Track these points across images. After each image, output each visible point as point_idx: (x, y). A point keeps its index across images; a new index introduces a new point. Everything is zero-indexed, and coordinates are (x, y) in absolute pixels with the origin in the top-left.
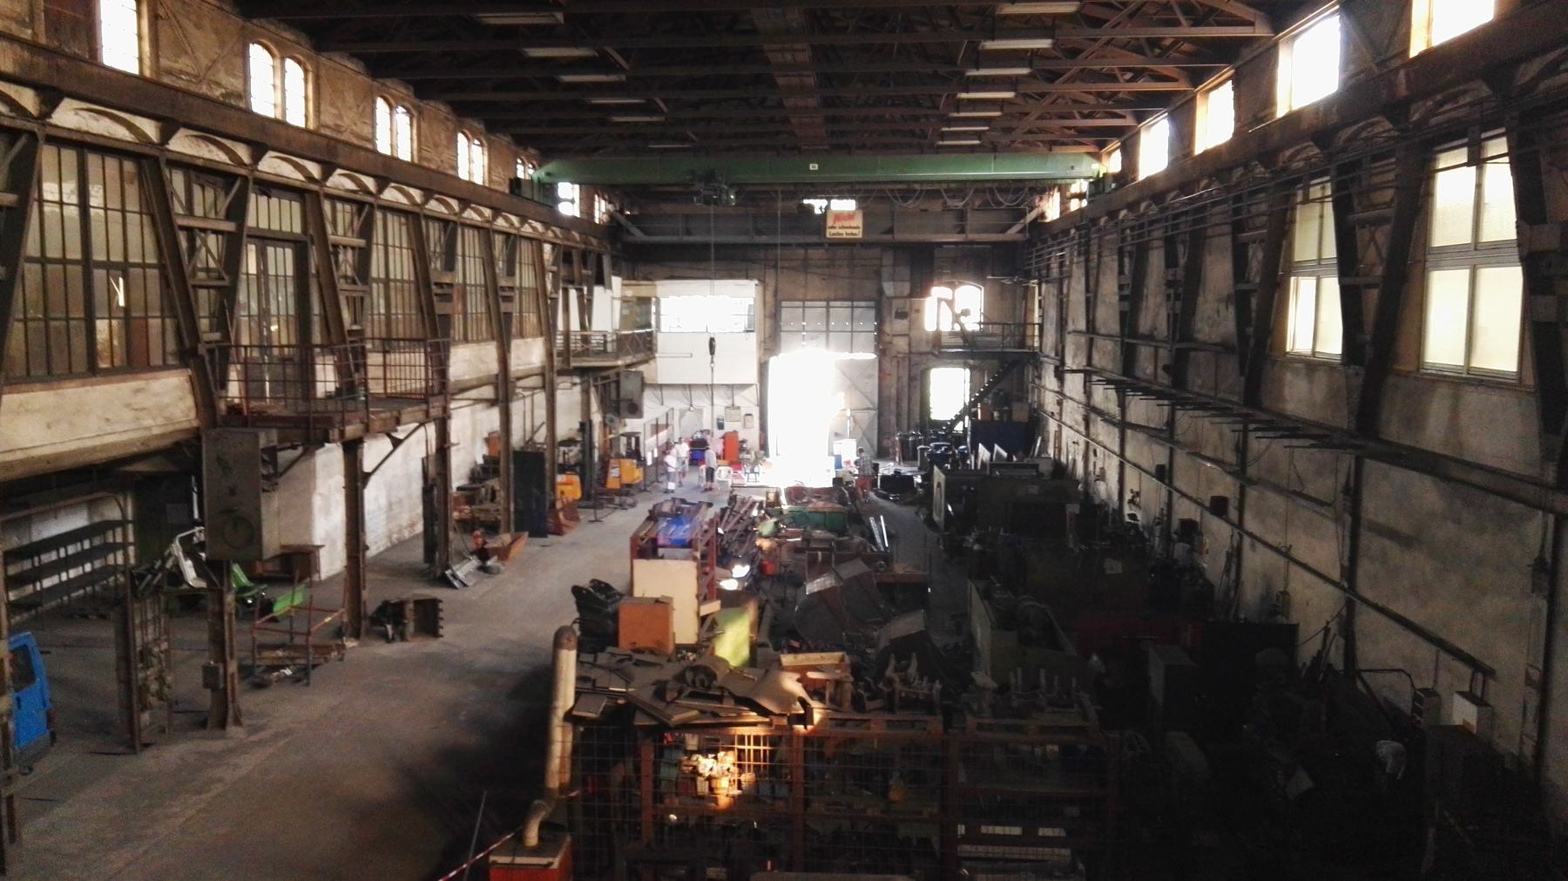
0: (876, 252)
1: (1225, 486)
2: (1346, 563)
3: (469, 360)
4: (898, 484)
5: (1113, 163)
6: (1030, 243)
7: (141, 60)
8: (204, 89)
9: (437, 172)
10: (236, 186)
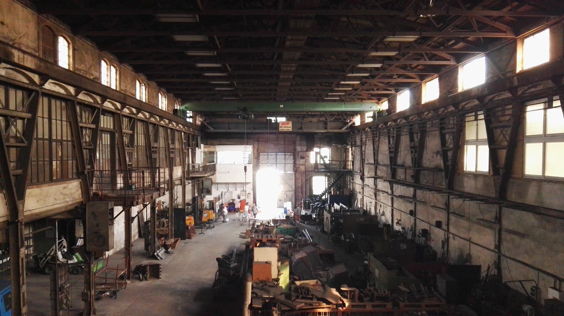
0: (294, 136)
1: (441, 216)
2: (497, 243)
3: (164, 174)
4: (306, 218)
5: (384, 106)
6: (348, 133)
7: (69, 65)
8: (88, 76)
9: (153, 106)
10: (96, 111)
